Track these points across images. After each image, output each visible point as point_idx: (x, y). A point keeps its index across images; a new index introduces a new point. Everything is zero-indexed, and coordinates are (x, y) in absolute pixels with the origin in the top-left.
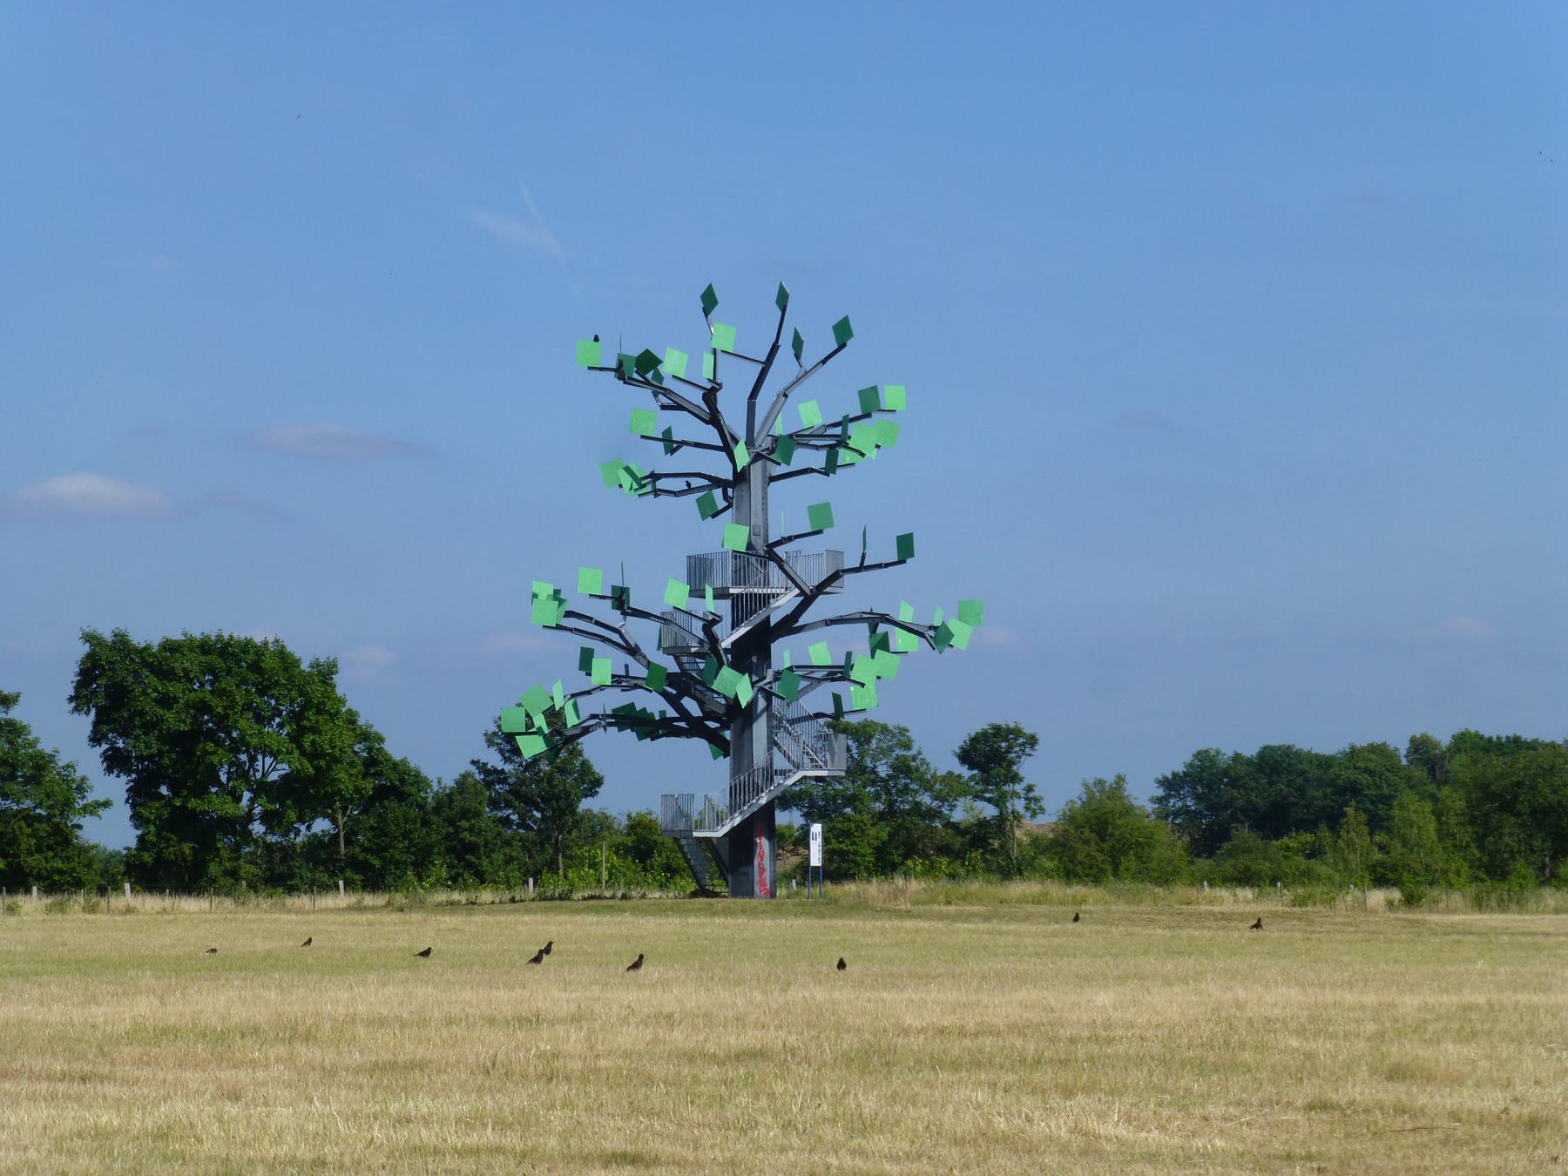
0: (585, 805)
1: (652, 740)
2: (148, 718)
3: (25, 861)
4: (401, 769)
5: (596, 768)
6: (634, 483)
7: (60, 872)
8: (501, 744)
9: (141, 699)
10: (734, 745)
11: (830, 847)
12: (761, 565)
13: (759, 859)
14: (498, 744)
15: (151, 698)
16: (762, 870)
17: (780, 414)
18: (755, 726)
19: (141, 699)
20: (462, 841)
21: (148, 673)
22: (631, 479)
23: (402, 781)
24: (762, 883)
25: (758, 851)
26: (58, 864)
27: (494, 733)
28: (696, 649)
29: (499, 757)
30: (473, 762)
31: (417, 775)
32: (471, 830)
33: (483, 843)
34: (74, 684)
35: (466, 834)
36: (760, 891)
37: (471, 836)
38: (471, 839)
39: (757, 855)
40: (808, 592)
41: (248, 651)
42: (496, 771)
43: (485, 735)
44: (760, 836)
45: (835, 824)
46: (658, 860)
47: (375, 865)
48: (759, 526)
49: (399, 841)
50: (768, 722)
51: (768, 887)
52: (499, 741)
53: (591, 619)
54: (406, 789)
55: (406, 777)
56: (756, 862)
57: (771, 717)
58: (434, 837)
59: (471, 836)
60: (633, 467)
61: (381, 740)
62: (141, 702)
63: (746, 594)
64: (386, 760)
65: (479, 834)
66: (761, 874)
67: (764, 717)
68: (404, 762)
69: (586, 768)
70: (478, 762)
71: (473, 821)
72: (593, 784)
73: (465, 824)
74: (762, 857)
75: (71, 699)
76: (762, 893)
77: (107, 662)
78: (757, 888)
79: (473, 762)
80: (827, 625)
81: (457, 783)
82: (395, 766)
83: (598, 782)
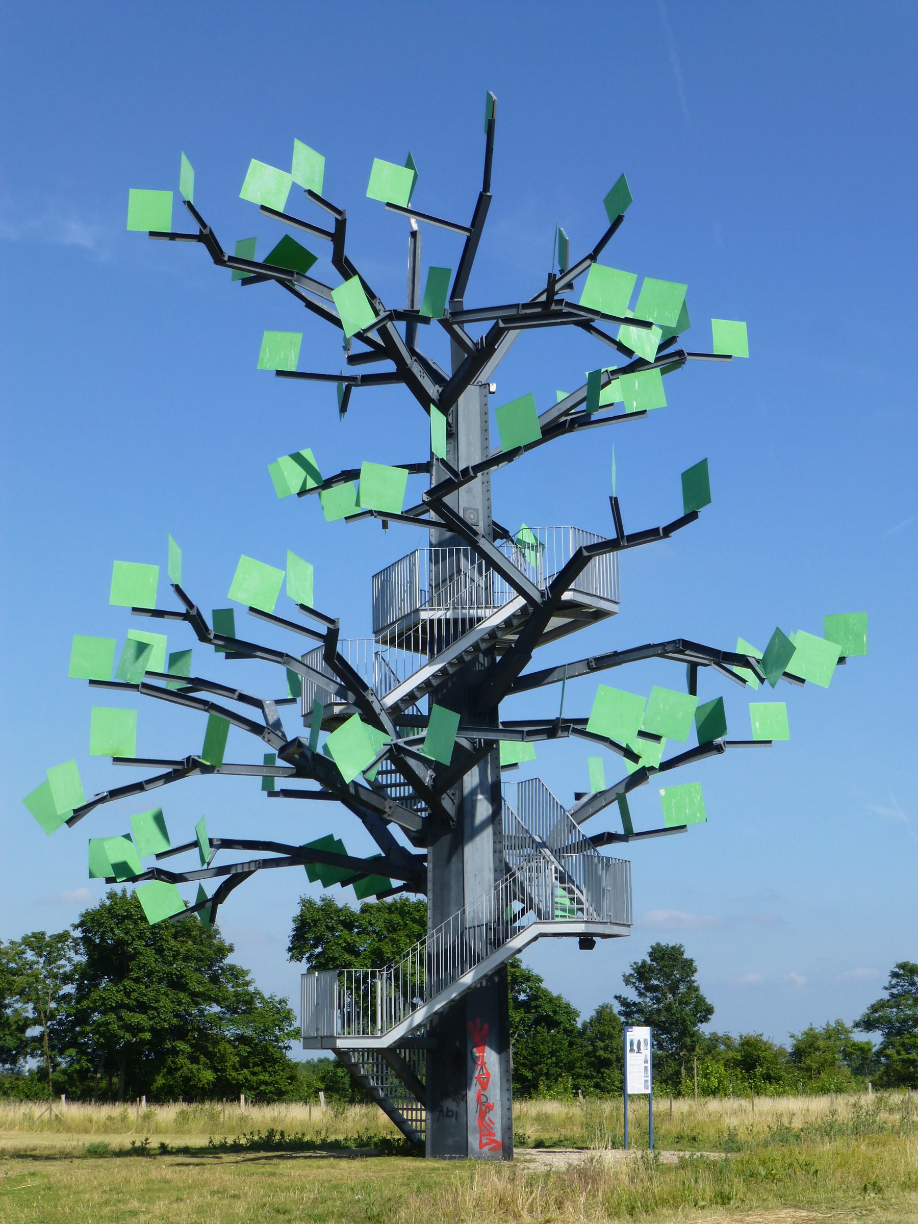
0: (705, 1029)
1: (343, 886)
2: (338, 963)
3: (230, 1075)
4: (555, 1003)
5: (709, 1001)
6: (308, 477)
7: (266, 1083)
8: (635, 983)
9: (333, 948)
10: (434, 885)
11: (901, 1057)
12: (480, 573)
13: (479, 1087)
14: (634, 983)
15: (341, 947)
16: (485, 1107)
17: (518, 331)
18: (469, 849)
19: (333, 948)
20: (598, 1058)
21: (342, 928)
22: (303, 473)
23: (555, 1012)
24: (485, 1130)
25: (476, 1074)
26: (265, 1077)
27: (631, 975)
28: (342, 707)
29: (636, 993)
30: (616, 997)
31: (567, 1006)
32: (605, 1049)
33: (615, 1059)
34: (291, 938)
35: (601, 1052)
36: (482, 1146)
37: (605, 1053)
38: (606, 1056)
39: (475, 1081)
40: (537, 597)
41: (420, 910)
42: (635, 1004)
43: (624, 976)
44: (481, 1044)
45: (904, 1040)
46: (759, 1070)
47: (527, 1077)
48: (477, 510)
49: (548, 1058)
50: (494, 842)
51: (498, 1137)
52: (634, 980)
53: (233, 691)
54: (557, 1017)
55: (558, 1009)
56: (472, 1094)
57: (498, 835)
58: (576, 1055)
59: (605, 1053)
60: (307, 454)
61: (539, 980)
62: (333, 950)
63: (439, 621)
64: (545, 996)
65: (611, 1052)
66: (482, 1115)
67: (487, 835)
68: (559, 998)
69: (701, 1000)
70: (620, 997)
71: (607, 1042)
72: (705, 1012)
73: (600, 1044)
74: (484, 1085)
75: (290, 950)
76: (486, 1148)
77: (312, 921)
78: (473, 1140)
79: (616, 997)
80: (592, 670)
81: (597, 1012)
82: (551, 1000)
83: (709, 1011)
